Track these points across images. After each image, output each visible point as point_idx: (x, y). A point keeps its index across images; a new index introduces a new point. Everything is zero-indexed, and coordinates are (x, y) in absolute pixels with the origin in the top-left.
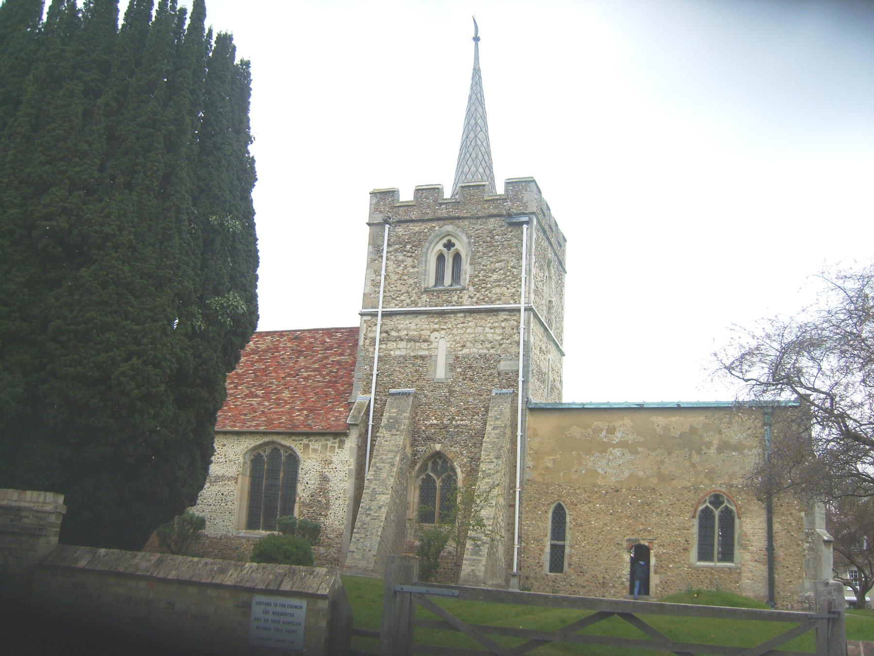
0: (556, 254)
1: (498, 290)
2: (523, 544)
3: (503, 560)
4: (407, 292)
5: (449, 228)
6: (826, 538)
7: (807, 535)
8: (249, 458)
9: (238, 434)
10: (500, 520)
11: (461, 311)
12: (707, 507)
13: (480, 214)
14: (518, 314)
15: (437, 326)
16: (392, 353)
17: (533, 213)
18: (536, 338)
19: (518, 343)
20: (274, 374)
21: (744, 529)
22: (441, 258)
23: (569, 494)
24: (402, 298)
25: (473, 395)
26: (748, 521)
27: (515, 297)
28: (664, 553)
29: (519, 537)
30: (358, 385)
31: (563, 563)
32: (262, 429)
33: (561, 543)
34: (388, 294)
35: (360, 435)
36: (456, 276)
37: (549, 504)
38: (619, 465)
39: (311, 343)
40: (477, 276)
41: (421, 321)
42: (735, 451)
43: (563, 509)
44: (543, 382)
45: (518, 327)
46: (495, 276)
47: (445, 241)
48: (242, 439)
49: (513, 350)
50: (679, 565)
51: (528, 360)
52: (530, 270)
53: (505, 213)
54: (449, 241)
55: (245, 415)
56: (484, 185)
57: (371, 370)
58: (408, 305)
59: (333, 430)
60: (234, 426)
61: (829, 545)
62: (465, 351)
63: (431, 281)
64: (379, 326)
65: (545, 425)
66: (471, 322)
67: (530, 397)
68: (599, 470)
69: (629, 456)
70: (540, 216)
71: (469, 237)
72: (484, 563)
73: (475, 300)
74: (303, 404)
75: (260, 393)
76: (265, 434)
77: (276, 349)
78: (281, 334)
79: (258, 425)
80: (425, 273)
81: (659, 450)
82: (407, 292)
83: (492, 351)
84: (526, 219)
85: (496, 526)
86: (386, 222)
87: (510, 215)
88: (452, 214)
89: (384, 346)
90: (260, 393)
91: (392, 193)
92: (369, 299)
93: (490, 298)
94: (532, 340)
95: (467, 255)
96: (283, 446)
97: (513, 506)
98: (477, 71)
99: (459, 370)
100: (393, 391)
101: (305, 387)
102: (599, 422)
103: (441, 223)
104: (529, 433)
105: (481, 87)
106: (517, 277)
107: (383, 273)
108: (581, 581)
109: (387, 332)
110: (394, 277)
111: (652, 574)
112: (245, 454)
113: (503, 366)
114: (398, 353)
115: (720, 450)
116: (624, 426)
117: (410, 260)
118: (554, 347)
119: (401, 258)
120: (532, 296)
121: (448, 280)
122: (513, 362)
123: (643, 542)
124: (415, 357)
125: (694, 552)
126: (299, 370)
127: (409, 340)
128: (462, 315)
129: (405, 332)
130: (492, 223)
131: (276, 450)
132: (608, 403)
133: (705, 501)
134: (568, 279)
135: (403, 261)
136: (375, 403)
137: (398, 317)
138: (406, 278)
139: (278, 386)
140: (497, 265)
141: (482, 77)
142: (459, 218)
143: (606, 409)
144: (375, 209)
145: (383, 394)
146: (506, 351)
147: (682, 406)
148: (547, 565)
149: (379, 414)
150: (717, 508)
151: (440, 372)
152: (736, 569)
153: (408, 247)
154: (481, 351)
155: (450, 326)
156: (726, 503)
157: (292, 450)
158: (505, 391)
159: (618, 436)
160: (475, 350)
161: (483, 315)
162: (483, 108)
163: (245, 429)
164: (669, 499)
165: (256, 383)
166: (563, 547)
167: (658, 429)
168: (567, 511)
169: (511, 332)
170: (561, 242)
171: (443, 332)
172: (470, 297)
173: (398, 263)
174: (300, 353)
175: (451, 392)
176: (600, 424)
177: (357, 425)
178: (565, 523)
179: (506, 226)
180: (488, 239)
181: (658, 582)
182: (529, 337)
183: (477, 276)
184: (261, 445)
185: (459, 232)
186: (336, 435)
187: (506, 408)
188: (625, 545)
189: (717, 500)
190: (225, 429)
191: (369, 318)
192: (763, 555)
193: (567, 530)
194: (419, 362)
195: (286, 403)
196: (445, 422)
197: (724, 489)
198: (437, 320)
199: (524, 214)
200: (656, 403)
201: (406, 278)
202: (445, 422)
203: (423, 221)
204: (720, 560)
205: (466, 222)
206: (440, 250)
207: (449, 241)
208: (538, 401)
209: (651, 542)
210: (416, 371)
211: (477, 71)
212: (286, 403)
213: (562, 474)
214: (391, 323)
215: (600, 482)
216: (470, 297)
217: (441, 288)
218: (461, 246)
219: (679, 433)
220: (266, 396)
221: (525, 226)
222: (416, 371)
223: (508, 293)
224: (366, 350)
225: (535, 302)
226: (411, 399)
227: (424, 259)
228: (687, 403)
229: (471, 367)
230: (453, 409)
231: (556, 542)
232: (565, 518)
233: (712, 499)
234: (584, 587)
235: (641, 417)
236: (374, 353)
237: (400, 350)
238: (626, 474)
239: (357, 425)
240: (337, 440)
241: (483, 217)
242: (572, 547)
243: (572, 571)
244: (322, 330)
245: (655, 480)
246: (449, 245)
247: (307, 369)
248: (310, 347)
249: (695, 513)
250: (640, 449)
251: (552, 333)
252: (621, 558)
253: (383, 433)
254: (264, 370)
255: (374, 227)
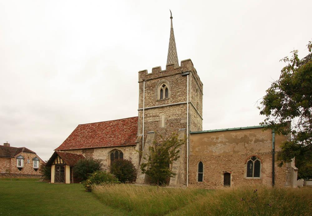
0: (199, 88)
1: (180, 98)
2: (190, 174)
3: (184, 179)
4: (152, 102)
5: (163, 80)
6: (295, 169)
7: (288, 168)
8: (110, 154)
9: (106, 148)
10: (182, 167)
11: (168, 106)
12: (250, 160)
13: (173, 74)
14: (186, 105)
15: (161, 111)
16: (148, 121)
17: (190, 71)
18: (192, 112)
19: (187, 114)
20: (117, 131)
21: (264, 167)
22: (162, 90)
23: (204, 159)
24: (150, 104)
25: (173, 131)
26: (265, 164)
27: (185, 100)
28: (235, 175)
29: (188, 172)
30: (139, 131)
31: (202, 179)
32: (112, 146)
33: (201, 173)
34: (146, 103)
35: (140, 146)
36: (166, 95)
37: (197, 162)
38: (220, 149)
39: (127, 122)
40: (173, 94)
41: (156, 110)
42: (261, 142)
43: (202, 163)
44: (196, 126)
45: (186, 109)
46: (179, 94)
47: (162, 84)
48: (107, 149)
49: (185, 116)
50: (240, 178)
51: (190, 119)
52: (190, 90)
53: (181, 72)
54: (164, 84)
55: (108, 142)
56: (174, 64)
57: (142, 126)
58: (152, 106)
59: (132, 145)
60: (104, 146)
61: (296, 171)
62: (170, 118)
63: (159, 98)
64: (144, 113)
65: (195, 138)
66: (171, 109)
67: (191, 130)
68: (213, 151)
69: (223, 146)
70: (193, 73)
71: (170, 82)
72: (176, 180)
73: (172, 102)
74: (124, 138)
75: (113, 136)
76: (113, 147)
77: (118, 124)
78: (119, 120)
79: (111, 145)
80: (157, 95)
81: (233, 144)
82: (152, 102)
83: (178, 117)
84: (188, 73)
85: (181, 169)
86: (144, 81)
87: (183, 73)
88: (164, 76)
89: (146, 119)
90: (113, 136)
91: (145, 71)
92: (140, 106)
93: (177, 101)
94: (191, 113)
95: (169, 88)
96: (118, 150)
97: (187, 163)
98: (172, 29)
99: (169, 124)
100: (149, 132)
101: (125, 133)
102: (213, 136)
103: (161, 79)
104: (190, 141)
105: (173, 35)
106: (186, 93)
107: (144, 97)
108: (208, 184)
109: (146, 115)
110: (147, 98)
111: (231, 181)
112: (108, 153)
113: (182, 122)
114: (150, 121)
115: (255, 142)
116: (222, 137)
117: (152, 92)
118: (199, 117)
119: (149, 92)
120: (191, 99)
121: (164, 97)
122: (185, 120)
123: (228, 172)
124: (155, 121)
125: (246, 174)
126: (124, 129)
127: (153, 117)
128: (169, 107)
129: (152, 114)
130: (177, 76)
131: (117, 151)
132: (216, 130)
133: (250, 159)
134: (204, 97)
135: (150, 93)
136: (144, 136)
137: (149, 110)
138: (151, 97)
139: (118, 134)
140: (179, 90)
141: (174, 31)
142: (166, 76)
143: (215, 132)
144: (140, 77)
145: (146, 133)
146: (183, 117)
147: (242, 128)
148: (197, 180)
149: (145, 139)
150: (254, 161)
151: (163, 125)
152: (261, 179)
153: (151, 88)
154: (175, 118)
155: (165, 111)
156: (257, 159)
157: (121, 151)
158: (183, 129)
159: (220, 140)
160: (173, 118)
161: (175, 106)
162: (175, 42)
163: (107, 146)
164: (237, 158)
165: (112, 134)
166: (202, 174)
167: (233, 137)
168: (203, 164)
169: (184, 111)
170: (201, 85)
171: (163, 113)
172: (171, 101)
173: (148, 93)
174: (124, 125)
175: (166, 131)
176: (214, 137)
177: (138, 142)
178: (203, 167)
179: (182, 76)
180: (176, 82)
181: (233, 184)
182: (190, 111)
183: (173, 94)
184: (112, 150)
185: (166, 81)
186: (133, 146)
187: (183, 134)
188: (222, 173)
189: (254, 158)
190: (102, 147)
191: (141, 111)
192: (271, 175)
193: (203, 169)
194: (156, 123)
195: (120, 138)
196: (165, 140)
197: (256, 154)
198: (161, 110)
199: (188, 72)
200: (233, 129)
201: (151, 97)
202: (165, 140)
203: (155, 79)
204: (255, 176)
205: (169, 77)
206: (161, 88)
207: (164, 84)
208: (193, 131)
209: (231, 172)
210: (156, 125)
211: (172, 29)
212: (120, 138)
213: (201, 153)
214: (147, 112)
215: (214, 154)
216: (171, 101)
217: (162, 100)
218: (167, 86)
219: (240, 137)
220: (115, 137)
221: (188, 76)
222: (156, 125)
223: (183, 98)
224: (141, 121)
225: (192, 101)
226: (154, 134)
227: (156, 91)
228: (244, 127)
229: (172, 123)
230: (167, 136)
231: (200, 173)
232: (202, 166)
233: (252, 158)
234: (209, 186)
235: (227, 133)
236: (143, 121)
237: (150, 120)
238: (222, 151)
239: (138, 142)
240: (133, 147)
241: (174, 75)
242: (205, 174)
243: (205, 181)
244: (130, 118)
245: (232, 153)
246: (164, 86)
247: (126, 129)
248: (127, 123)
249: (246, 162)
250: (227, 144)
251: (198, 112)
252: (221, 177)
253: (146, 144)
254: (114, 130)
255: (140, 83)
